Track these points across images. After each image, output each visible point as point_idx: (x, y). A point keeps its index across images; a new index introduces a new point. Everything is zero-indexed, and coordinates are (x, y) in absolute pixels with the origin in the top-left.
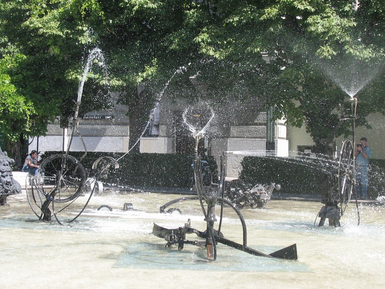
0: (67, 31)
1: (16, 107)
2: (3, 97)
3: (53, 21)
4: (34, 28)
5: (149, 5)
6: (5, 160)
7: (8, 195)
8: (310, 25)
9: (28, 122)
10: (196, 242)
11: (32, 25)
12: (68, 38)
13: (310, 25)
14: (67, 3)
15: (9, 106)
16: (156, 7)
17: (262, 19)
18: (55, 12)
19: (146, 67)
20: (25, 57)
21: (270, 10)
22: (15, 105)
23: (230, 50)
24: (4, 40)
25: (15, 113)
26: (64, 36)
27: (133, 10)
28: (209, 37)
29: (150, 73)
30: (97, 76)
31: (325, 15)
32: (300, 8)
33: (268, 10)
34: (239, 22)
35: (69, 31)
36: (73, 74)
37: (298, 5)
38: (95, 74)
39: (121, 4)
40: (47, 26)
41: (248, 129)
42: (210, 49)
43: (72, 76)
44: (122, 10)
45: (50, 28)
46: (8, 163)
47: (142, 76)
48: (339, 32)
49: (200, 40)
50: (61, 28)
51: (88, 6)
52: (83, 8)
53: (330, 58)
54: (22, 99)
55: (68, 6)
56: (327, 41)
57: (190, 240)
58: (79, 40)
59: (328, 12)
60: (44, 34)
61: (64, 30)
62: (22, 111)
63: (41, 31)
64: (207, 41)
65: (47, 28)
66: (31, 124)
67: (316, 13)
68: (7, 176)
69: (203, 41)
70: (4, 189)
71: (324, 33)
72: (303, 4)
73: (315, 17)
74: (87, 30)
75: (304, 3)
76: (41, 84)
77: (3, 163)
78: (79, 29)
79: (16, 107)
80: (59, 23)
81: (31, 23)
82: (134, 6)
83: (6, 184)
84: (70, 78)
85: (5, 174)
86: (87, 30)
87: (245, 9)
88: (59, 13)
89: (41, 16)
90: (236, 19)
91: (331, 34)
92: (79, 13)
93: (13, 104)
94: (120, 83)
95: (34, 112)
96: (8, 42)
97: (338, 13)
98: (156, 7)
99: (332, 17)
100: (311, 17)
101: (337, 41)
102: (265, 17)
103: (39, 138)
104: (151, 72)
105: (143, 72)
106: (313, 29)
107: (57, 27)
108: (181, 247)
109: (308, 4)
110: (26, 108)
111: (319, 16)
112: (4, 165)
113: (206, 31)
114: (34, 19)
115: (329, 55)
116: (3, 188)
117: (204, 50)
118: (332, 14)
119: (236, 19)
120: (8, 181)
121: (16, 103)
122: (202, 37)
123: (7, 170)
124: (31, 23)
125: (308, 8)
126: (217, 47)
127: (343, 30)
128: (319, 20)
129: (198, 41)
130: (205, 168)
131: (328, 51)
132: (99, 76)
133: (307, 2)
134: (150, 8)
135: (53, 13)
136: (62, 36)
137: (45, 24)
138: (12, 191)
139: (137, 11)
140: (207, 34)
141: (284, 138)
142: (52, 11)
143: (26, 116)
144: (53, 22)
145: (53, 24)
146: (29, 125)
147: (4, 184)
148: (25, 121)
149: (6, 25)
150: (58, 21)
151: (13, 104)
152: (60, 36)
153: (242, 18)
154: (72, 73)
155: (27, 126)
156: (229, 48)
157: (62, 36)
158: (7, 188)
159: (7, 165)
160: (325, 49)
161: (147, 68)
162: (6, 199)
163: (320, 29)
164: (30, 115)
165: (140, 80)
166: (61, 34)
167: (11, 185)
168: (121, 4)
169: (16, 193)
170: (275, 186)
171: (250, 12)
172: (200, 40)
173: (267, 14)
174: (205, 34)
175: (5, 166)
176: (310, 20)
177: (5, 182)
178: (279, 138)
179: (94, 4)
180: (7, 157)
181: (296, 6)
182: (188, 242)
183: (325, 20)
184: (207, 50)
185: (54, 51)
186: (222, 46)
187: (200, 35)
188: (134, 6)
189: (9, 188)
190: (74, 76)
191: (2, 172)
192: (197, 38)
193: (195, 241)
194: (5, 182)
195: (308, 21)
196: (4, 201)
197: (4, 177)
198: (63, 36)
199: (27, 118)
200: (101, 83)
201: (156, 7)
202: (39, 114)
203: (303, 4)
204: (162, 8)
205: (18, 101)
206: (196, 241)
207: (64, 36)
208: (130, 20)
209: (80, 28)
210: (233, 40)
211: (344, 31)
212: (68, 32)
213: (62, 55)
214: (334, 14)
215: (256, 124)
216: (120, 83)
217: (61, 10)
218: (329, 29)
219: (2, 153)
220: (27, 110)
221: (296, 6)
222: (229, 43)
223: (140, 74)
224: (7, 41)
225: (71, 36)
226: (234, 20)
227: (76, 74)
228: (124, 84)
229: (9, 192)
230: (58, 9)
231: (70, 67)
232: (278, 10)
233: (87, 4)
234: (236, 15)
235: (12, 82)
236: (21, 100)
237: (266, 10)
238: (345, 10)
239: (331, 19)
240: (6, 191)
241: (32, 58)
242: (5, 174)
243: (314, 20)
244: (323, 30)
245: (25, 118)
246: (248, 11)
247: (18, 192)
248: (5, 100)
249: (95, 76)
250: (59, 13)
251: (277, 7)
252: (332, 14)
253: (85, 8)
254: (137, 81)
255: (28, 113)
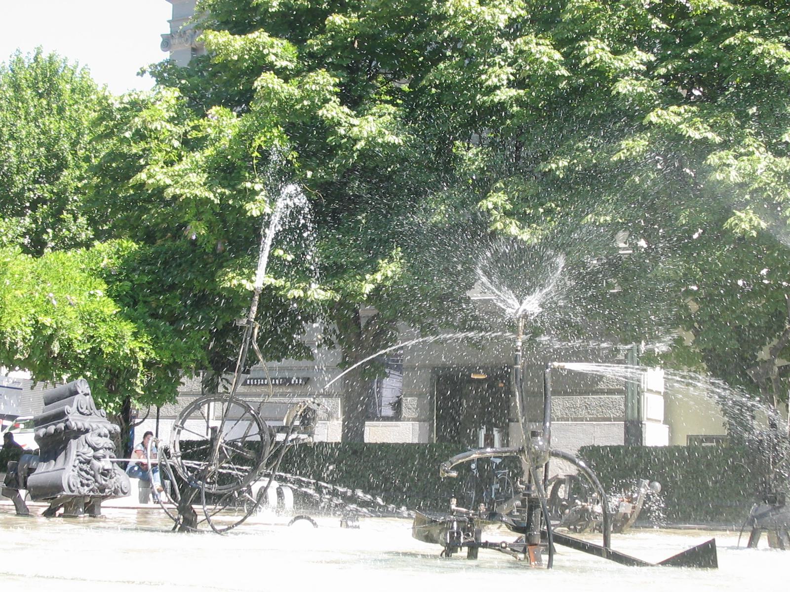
0: (223, 190)
1: (117, 343)
2: (91, 324)
3: (195, 172)
4: (156, 187)
5: (386, 138)
6: (100, 425)
7: (104, 498)
8: (712, 169)
9: (139, 375)
10: (504, 545)
11: (150, 181)
12: (224, 205)
13: (712, 169)
14: (223, 136)
15: (101, 342)
16: (402, 144)
17: (615, 158)
18: (198, 156)
19: (380, 261)
20: (135, 246)
21: (631, 142)
22: (114, 340)
23: (551, 225)
24: (86, 235)
25: (113, 356)
26: (217, 201)
27: (354, 149)
28: (507, 200)
29: (390, 274)
30: (280, 282)
31: (742, 150)
32: (692, 136)
33: (627, 142)
34: (569, 169)
35: (227, 192)
36: (233, 278)
37: (687, 132)
38: (276, 279)
39: (331, 138)
40: (182, 182)
41: (585, 402)
42: (511, 223)
43: (231, 280)
44: (331, 151)
45: (190, 185)
46: (107, 432)
47: (374, 280)
48: (772, 182)
49: (491, 206)
50: (209, 185)
51: (265, 142)
52: (256, 144)
53: (754, 234)
54: (129, 326)
55: (224, 143)
56: (747, 202)
57: (491, 540)
58: (247, 209)
59: (748, 145)
60: (175, 198)
61: (216, 189)
62: (129, 352)
63: (169, 192)
64: (504, 208)
65: (183, 186)
66: (145, 380)
67: (725, 145)
68: (104, 457)
69: (496, 207)
70: (97, 484)
71: (741, 186)
72: (699, 129)
73: (723, 154)
74: (262, 190)
75: (701, 127)
76: (167, 299)
77: (97, 432)
78: (245, 188)
79: (117, 343)
80: (206, 175)
81: (150, 177)
82: (356, 141)
83: (103, 474)
84: (227, 285)
85: (100, 453)
86: (262, 190)
87: (580, 144)
88: (205, 157)
89: (169, 163)
90: (564, 163)
91: (756, 186)
92: (247, 157)
93: (110, 337)
94: (329, 295)
95: (153, 356)
96: (93, 239)
97: (769, 147)
98: (401, 141)
99: (757, 153)
100: (715, 154)
101: (768, 199)
102: (622, 155)
103: (161, 409)
104: (392, 271)
105: (375, 271)
106: (719, 176)
107: (202, 183)
108: (472, 555)
109: (709, 128)
110: (135, 345)
111: (731, 152)
112: (99, 435)
113: (501, 189)
114: (156, 169)
115: (751, 229)
116: (96, 481)
117: (499, 225)
118: (757, 148)
119: (564, 163)
120: (106, 468)
121: (116, 335)
122: (494, 199)
123: (105, 446)
124: (150, 177)
125: (710, 135)
126: (525, 220)
127: (779, 178)
128: (731, 160)
129: (487, 208)
130: (499, 473)
131: (751, 220)
132: (286, 282)
133: (705, 126)
134: (388, 144)
135: (194, 159)
136: (213, 201)
137: (176, 178)
138: (113, 489)
139: (362, 153)
140: (504, 194)
141: (660, 421)
142: (192, 154)
143: (136, 362)
144: (195, 175)
145: (193, 178)
146: (142, 381)
147: (97, 473)
148: (134, 374)
149: (97, 186)
150: (204, 171)
151: (110, 337)
152: (208, 200)
153: (575, 161)
154: (230, 275)
155: (138, 382)
156: (550, 221)
157: (213, 201)
158: (104, 482)
159: (106, 436)
160: (743, 215)
161: (383, 263)
162: (99, 506)
163: (734, 177)
164: (144, 361)
165: (368, 288)
166: (211, 196)
167: (111, 478)
168: (331, 138)
169: (121, 494)
170: (649, 485)
171: (590, 151)
172: (491, 206)
173: (625, 151)
174: (500, 194)
175: (101, 437)
176: (712, 159)
177: (99, 469)
178: (648, 419)
179: (277, 137)
180: (105, 420)
181: (684, 134)
182: (486, 545)
183: (743, 161)
184: (504, 224)
185: (196, 231)
186: (535, 219)
187: (490, 195)
188: (356, 141)
189: (107, 483)
190: (235, 282)
191: (95, 449)
192: (484, 201)
193: (501, 543)
194: (99, 469)
195: (708, 162)
196: (96, 509)
197: (98, 459)
198: (216, 200)
199: (138, 365)
200: (289, 295)
201: (402, 144)
202: (162, 359)
203: (699, 129)
204: (413, 146)
205: (121, 332)
206: (504, 542)
207: (217, 201)
208: (347, 172)
209: (248, 185)
210: (557, 206)
211: (782, 181)
212: (225, 193)
213: (212, 238)
214: (762, 149)
215: (602, 392)
216: (329, 295)
217: (209, 151)
218: (752, 176)
219: (96, 411)
220: (137, 350)
221: (684, 134)
222: (549, 212)
223: (368, 276)
224: (92, 237)
225: (231, 202)
226: (558, 166)
227: (240, 278)
228: (335, 297)
229: (107, 490)
230: (202, 149)
231: (225, 264)
232: (647, 143)
233: (263, 139)
234: (563, 154)
235: (109, 293)
236: (128, 328)
237: (624, 144)
238: (784, 141)
239: (755, 157)
240: (102, 489)
241: (150, 250)
242: (100, 453)
243: (720, 158)
244: (739, 180)
245: (135, 367)
246: (586, 149)
247: (125, 493)
248: (96, 328)
249: (278, 281)
250: (205, 157)
251: (646, 137)
252: (757, 148)
253: (260, 146)
254: (363, 291)
255: (141, 356)
